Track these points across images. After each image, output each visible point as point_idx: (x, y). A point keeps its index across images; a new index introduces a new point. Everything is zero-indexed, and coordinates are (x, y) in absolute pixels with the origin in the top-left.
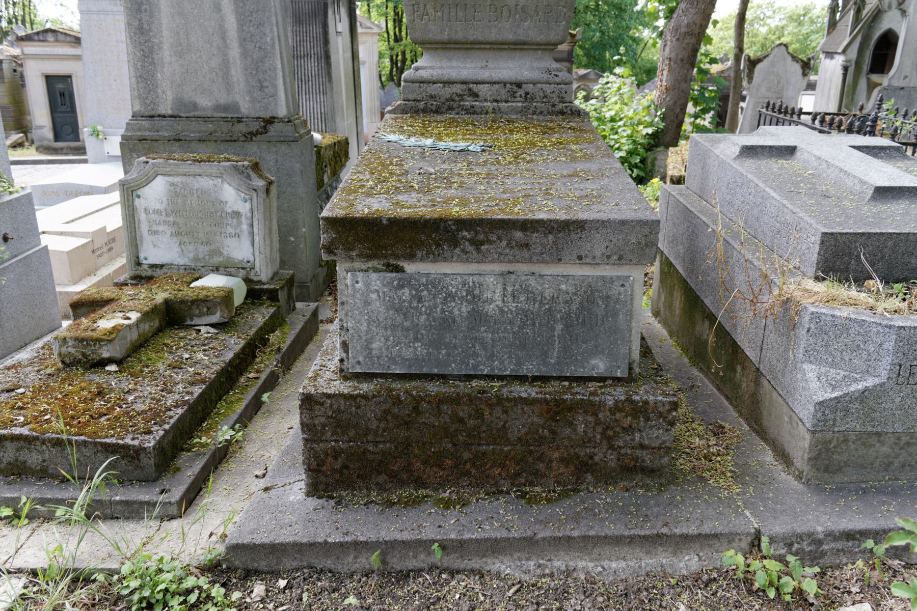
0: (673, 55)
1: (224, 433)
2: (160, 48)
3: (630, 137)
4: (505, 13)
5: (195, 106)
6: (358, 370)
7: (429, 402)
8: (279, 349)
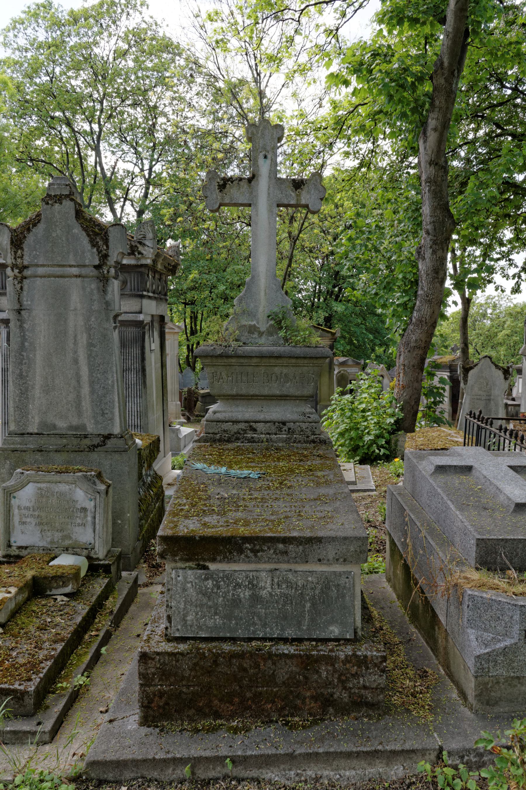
0: (406, 362)
1: (80, 680)
2: (33, 388)
3: (377, 423)
4: (274, 378)
5: (54, 427)
6: (177, 635)
7: (224, 657)
8: (112, 612)
